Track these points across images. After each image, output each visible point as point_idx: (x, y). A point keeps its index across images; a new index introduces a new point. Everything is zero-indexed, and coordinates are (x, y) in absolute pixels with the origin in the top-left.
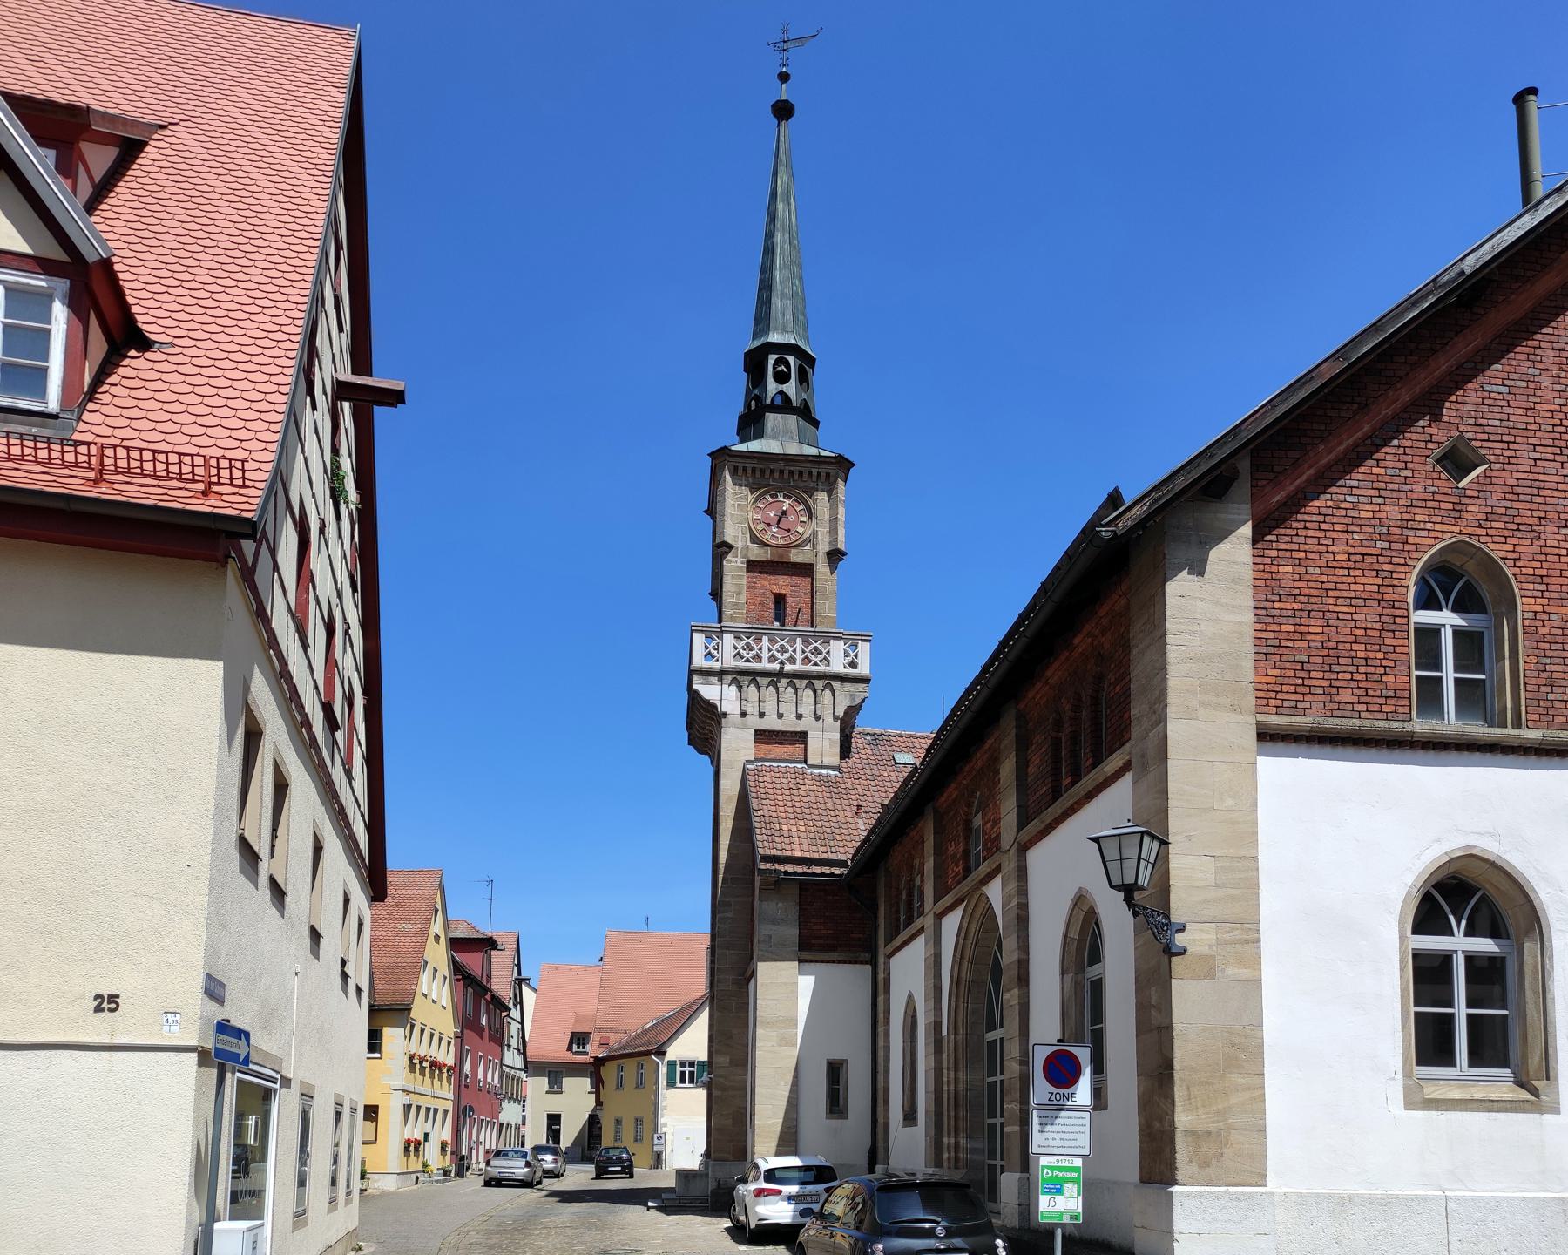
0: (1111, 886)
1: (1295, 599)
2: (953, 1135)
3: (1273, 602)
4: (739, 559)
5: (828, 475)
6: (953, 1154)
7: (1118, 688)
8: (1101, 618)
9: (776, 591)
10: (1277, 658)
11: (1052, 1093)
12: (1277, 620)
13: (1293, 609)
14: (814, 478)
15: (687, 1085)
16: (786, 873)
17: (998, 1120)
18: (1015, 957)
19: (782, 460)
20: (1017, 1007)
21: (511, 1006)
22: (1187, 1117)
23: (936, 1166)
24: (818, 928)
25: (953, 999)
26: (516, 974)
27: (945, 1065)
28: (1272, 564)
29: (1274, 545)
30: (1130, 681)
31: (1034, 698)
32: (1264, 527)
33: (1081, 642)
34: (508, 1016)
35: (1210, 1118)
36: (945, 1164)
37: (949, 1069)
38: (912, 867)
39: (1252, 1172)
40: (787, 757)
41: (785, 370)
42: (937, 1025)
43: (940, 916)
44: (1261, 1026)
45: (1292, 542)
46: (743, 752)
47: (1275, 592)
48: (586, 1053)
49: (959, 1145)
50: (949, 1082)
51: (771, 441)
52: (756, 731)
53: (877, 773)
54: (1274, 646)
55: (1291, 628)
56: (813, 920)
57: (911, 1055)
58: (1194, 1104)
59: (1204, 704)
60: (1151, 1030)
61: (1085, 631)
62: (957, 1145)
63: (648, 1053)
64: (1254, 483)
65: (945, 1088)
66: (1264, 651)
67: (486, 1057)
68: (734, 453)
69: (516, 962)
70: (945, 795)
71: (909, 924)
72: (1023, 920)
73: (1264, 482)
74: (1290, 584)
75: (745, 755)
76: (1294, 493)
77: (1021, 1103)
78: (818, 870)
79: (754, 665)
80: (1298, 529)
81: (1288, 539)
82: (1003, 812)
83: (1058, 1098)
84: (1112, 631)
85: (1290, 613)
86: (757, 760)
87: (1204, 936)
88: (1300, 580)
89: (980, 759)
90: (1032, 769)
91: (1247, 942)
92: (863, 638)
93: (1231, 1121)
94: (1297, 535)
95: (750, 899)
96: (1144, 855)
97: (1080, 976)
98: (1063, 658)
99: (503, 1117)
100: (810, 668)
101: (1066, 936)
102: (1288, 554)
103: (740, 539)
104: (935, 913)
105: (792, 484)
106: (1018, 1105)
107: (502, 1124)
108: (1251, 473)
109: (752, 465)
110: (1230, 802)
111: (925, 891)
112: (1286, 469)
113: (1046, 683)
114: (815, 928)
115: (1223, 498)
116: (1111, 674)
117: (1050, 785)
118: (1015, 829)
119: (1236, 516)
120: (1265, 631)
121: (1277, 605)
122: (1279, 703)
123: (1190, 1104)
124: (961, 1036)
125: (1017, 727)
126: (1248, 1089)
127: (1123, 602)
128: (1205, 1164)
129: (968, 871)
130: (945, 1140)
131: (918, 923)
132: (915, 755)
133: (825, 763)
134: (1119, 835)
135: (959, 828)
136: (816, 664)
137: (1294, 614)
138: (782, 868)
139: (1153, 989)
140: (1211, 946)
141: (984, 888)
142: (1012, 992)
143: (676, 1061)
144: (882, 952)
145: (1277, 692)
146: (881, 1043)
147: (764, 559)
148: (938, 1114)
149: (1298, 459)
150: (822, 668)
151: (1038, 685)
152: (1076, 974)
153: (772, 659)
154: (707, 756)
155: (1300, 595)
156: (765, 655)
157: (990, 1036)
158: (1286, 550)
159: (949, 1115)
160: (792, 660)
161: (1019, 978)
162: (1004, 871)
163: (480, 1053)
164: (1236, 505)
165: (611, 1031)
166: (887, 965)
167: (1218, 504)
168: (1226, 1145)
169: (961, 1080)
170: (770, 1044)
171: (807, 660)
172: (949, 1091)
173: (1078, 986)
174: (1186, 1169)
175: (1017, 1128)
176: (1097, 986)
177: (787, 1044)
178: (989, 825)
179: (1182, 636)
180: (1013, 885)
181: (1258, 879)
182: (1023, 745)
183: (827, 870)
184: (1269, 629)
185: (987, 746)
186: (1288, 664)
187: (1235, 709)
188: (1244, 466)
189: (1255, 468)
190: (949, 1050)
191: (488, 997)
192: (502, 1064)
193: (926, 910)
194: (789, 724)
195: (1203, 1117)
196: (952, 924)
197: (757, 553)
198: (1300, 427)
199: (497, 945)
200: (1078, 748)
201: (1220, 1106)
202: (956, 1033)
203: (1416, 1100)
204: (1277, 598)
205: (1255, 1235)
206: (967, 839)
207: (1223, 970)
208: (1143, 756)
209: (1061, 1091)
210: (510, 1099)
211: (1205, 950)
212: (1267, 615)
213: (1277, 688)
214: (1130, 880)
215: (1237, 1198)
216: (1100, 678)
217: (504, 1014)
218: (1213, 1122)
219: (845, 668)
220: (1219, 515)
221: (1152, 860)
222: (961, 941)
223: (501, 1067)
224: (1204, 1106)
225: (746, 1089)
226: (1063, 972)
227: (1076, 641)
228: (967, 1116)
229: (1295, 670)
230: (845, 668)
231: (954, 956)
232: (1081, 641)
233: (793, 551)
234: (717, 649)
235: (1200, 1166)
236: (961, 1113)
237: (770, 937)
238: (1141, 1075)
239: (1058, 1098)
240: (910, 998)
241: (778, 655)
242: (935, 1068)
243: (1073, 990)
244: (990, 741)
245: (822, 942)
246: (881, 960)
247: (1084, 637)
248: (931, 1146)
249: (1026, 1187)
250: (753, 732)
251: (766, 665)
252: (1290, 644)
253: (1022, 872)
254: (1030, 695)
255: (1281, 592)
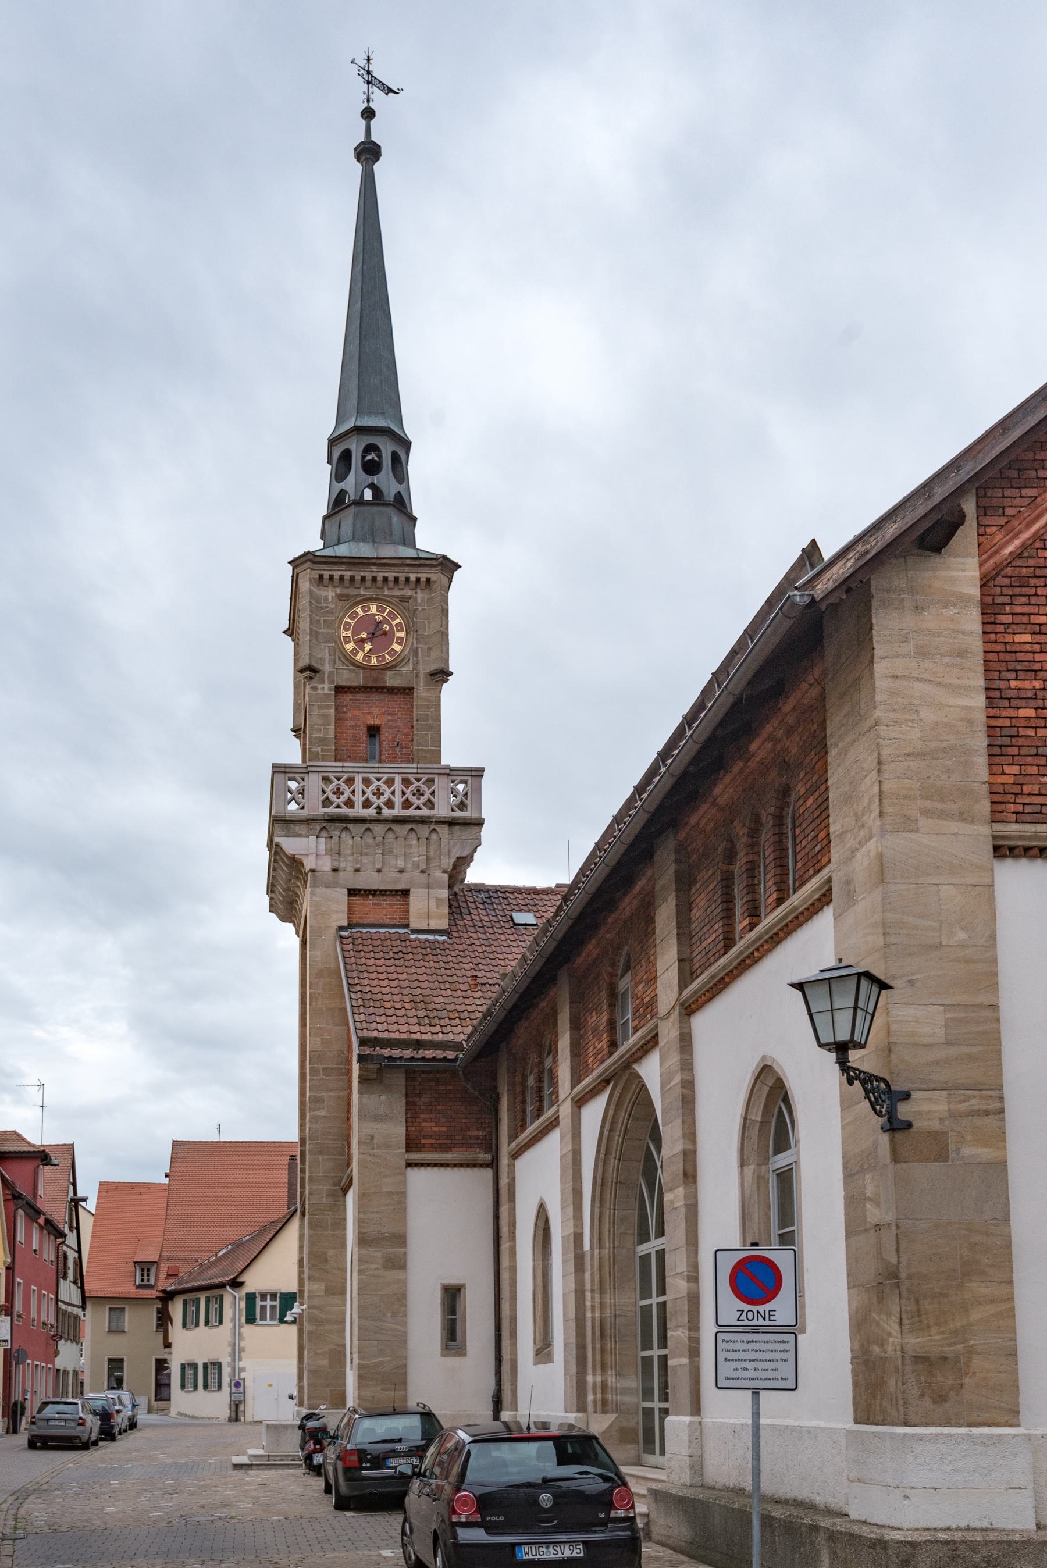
0: (821, 1045)
1: (1035, 675)
2: (599, 1372)
3: (1009, 680)
4: (326, 686)
5: (428, 580)
6: (599, 1396)
7: (810, 801)
8: (786, 715)
9: (371, 722)
10: (1015, 751)
11: (743, 1311)
12: (1014, 703)
13: (1034, 688)
14: (413, 585)
15: (268, 1321)
16: (390, 1058)
17: (655, 1353)
18: (679, 1147)
19: (374, 564)
20: (683, 1210)
21: (66, 1230)
22: (917, 1338)
23: (578, 1411)
24: (429, 1124)
25: (597, 1204)
26: (71, 1194)
27: (588, 1286)
28: (1005, 633)
29: (1008, 608)
30: (827, 788)
31: (698, 824)
32: (995, 586)
33: (759, 748)
34: (63, 1243)
35: (946, 1339)
36: (590, 1408)
37: (592, 1291)
38: (540, 1047)
39: (1000, 1408)
40: (387, 921)
41: (376, 459)
42: (578, 1237)
43: (580, 1102)
44: (1006, 1219)
45: (1029, 604)
46: (335, 916)
47: (1010, 668)
48: (151, 1287)
49: (607, 1385)
50: (593, 1308)
51: (361, 544)
52: (349, 890)
53: (493, 937)
54: (1011, 737)
55: (1032, 713)
56: (422, 1116)
57: (544, 1276)
58: (925, 1321)
59: (926, 813)
60: (866, 1230)
61: (764, 734)
62: (604, 1386)
63: (222, 1286)
64: (982, 529)
65: (589, 1315)
66: (999, 743)
67: (39, 1291)
68: (318, 559)
69: (71, 1180)
70: (584, 954)
71: (538, 1116)
72: (688, 1101)
73: (994, 529)
74: (1030, 657)
75: (336, 921)
76: (1031, 541)
77: (690, 1330)
78: (429, 1054)
79: (345, 811)
80: (1036, 587)
81: (1024, 600)
82: (660, 967)
83: (750, 1317)
84: (800, 729)
85: (1030, 694)
86: (350, 926)
87: (933, 1107)
88: (1041, 652)
89: (628, 905)
90: (696, 913)
91: (987, 1113)
92: (474, 773)
93: (972, 1342)
94: (1036, 595)
95: (345, 1093)
96: (861, 1004)
97: (764, 1168)
98: (736, 769)
99: (60, 1362)
100: (411, 812)
101: (745, 1119)
102: (1025, 619)
103: (327, 660)
104: (572, 1099)
105: (386, 593)
106: (687, 1333)
107: (58, 1370)
108: (977, 518)
109: (340, 573)
110: (962, 935)
111: (560, 1073)
112: (1020, 512)
113: (714, 803)
114: (425, 1124)
115: (943, 551)
116: (800, 785)
117: (720, 931)
118: (676, 989)
119: (961, 573)
120: (1000, 717)
121: (1013, 684)
122: (1020, 808)
123: (920, 1321)
124: (607, 1251)
125: (677, 861)
126: (993, 1301)
127: (815, 692)
128: (941, 1399)
129: (613, 1045)
130: (590, 1379)
131: (549, 1113)
132: (538, 915)
133: (432, 927)
134: (829, 979)
135: (601, 994)
136: (418, 808)
137: (1035, 694)
138: (387, 1052)
139: (868, 1177)
140: (941, 1120)
141: (635, 1066)
142: (675, 1191)
143: (255, 1294)
144: (505, 1150)
145: (1016, 794)
146: (505, 1262)
147: (356, 684)
148: (581, 1347)
149: (1036, 497)
150: (425, 812)
151: (705, 807)
152: (759, 1165)
153: (367, 804)
154: (291, 924)
155: (1041, 670)
156: (359, 799)
157: (643, 1249)
158: (1023, 614)
159: (594, 1349)
160: (390, 804)
161: (685, 1174)
162: (662, 1041)
163: (34, 1287)
164: (959, 559)
165: (180, 1259)
166: (511, 1167)
167: (938, 560)
168: (967, 1374)
169: (608, 1304)
170: (374, 1266)
171: (407, 804)
172: (593, 1319)
173: (761, 1180)
174: (917, 1406)
175: (685, 1361)
176: (786, 1179)
177: (394, 1267)
178: (640, 987)
179: (897, 728)
180: (674, 1059)
181: (999, 1033)
182: (685, 882)
183: (440, 1054)
184: (1004, 714)
185: (637, 889)
186: (1030, 758)
187: (965, 817)
188: (970, 507)
189: (983, 511)
190: (592, 1267)
191: (41, 1220)
192: (57, 1300)
193: (562, 1097)
194: (389, 880)
195: (937, 1337)
196: (594, 1113)
197: (348, 678)
198: (1037, 457)
199: (50, 1159)
200: (756, 882)
201: (959, 1324)
202: (601, 1247)
203: (442, 1355)
204: (1012, 675)
205: (1007, 1489)
206: (612, 1006)
207: (958, 1150)
208: (848, 882)
209: (755, 1308)
210: (66, 1340)
211: (935, 1125)
212: (1002, 698)
213: (1017, 790)
214: (843, 1036)
215: (985, 1442)
216: (785, 792)
217: (59, 1240)
218: (950, 1345)
219: (453, 810)
220: (937, 573)
221: (870, 1010)
222: (606, 1133)
223: (57, 1303)
224: (937, 1324)
225: (345, 1322)
226: (743, 1163)
227: (753, 747)
228: (615, 1348)
229: (1038, 766)
230: (453, 810)
231: (598, 1151)
232: (759, 748)
233: (389, 673)
234: (302, 794)
235: (934, 1402)
236: (609, 1345)
237: (372, 1137)
238: (854, 1286)
239: (750, 1317)
240: (542, 1208)
241: (373, 799)
242: (576, 1291)
243: (756, 1186)
244: (641, 883)
245: (433, 1141)
246: (504, 1161)
247: (764, 742)
248: (572, 1387)
249: (698, 1434)
250: (345, 891)
251: (359, 811)
252: (1031, 732)
253: (686, 1041)
254: (693, 820)
255: (1018, 667)
